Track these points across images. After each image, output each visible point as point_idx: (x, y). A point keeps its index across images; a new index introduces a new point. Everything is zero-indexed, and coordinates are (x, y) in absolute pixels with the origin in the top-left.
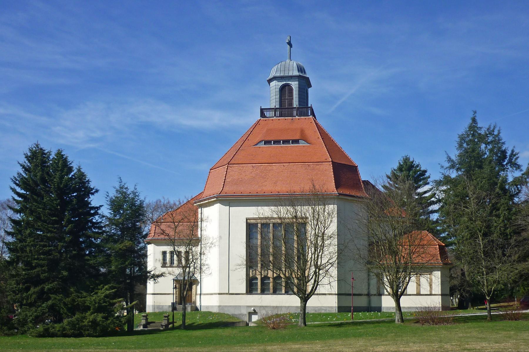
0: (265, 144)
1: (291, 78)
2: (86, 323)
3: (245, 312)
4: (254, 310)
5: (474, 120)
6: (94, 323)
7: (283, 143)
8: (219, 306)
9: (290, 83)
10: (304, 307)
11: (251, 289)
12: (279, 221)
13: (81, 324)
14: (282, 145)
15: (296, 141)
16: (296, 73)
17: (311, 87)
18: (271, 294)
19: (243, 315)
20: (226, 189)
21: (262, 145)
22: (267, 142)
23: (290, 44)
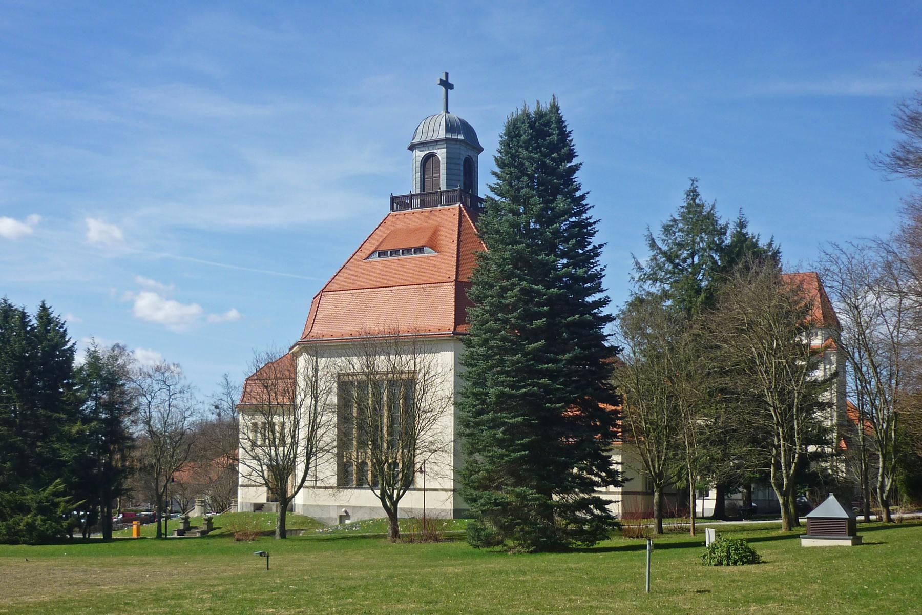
0: (379, 256)
1: (437, 142)
2: (21, 527)
3: (335, 515)
4: (346, 512)
5: (693, 194)
6: (31, 527)
7: (403, 254)
8: (304, 505)
9: (435, 151)
10: (392, 512)
11: (344, 482)
12: (364, 377)
13: (18, 528)
14: (390, 258)
15: (419, 250)
16: (442, 135)
17: (482, 149)
18: (355, 488)
19: (332, 519)
20: (316, 330)
21: (375, 258)
22: (382, 254)
23: (447, 85)
